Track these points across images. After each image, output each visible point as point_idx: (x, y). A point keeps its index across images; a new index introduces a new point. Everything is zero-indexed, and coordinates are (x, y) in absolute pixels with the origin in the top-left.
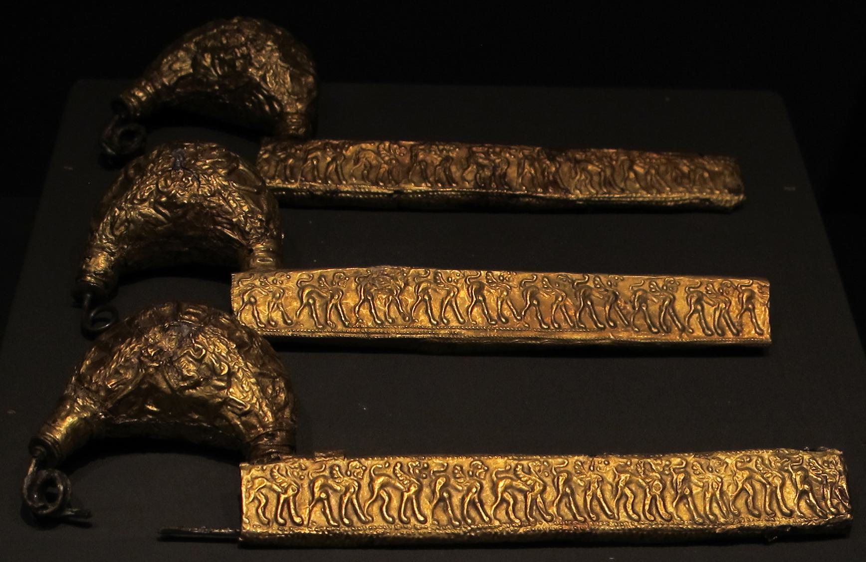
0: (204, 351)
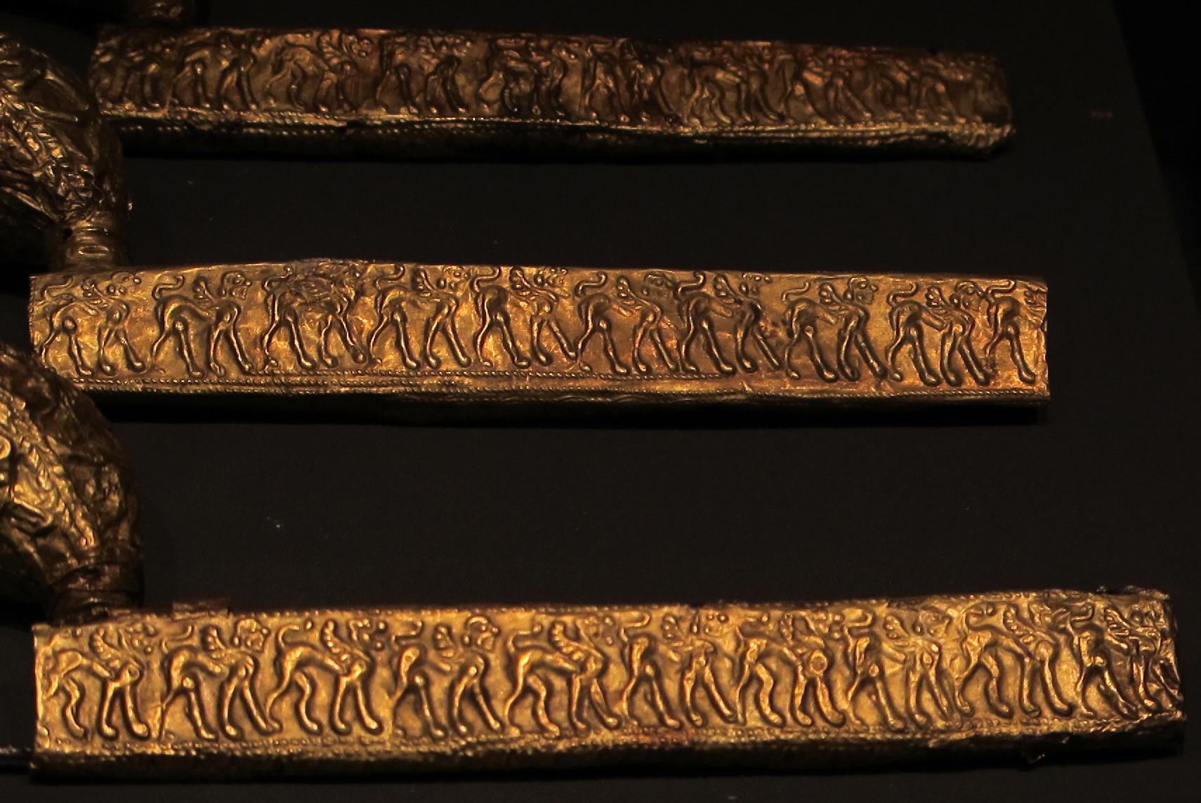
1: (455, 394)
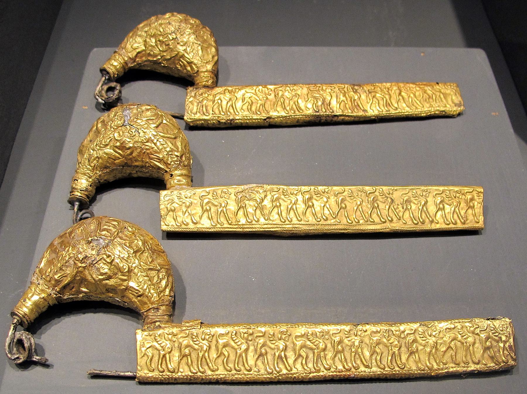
0: (113, 256)
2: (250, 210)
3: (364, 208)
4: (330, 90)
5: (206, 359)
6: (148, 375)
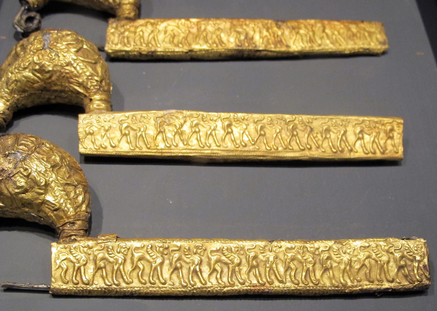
0: (30, 170)
1: (215, 156)
2: (170, 135)
3: (284, 136)
4: (253, 25)
5: (121, 272)
6: (62, 287)
